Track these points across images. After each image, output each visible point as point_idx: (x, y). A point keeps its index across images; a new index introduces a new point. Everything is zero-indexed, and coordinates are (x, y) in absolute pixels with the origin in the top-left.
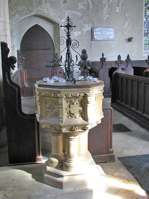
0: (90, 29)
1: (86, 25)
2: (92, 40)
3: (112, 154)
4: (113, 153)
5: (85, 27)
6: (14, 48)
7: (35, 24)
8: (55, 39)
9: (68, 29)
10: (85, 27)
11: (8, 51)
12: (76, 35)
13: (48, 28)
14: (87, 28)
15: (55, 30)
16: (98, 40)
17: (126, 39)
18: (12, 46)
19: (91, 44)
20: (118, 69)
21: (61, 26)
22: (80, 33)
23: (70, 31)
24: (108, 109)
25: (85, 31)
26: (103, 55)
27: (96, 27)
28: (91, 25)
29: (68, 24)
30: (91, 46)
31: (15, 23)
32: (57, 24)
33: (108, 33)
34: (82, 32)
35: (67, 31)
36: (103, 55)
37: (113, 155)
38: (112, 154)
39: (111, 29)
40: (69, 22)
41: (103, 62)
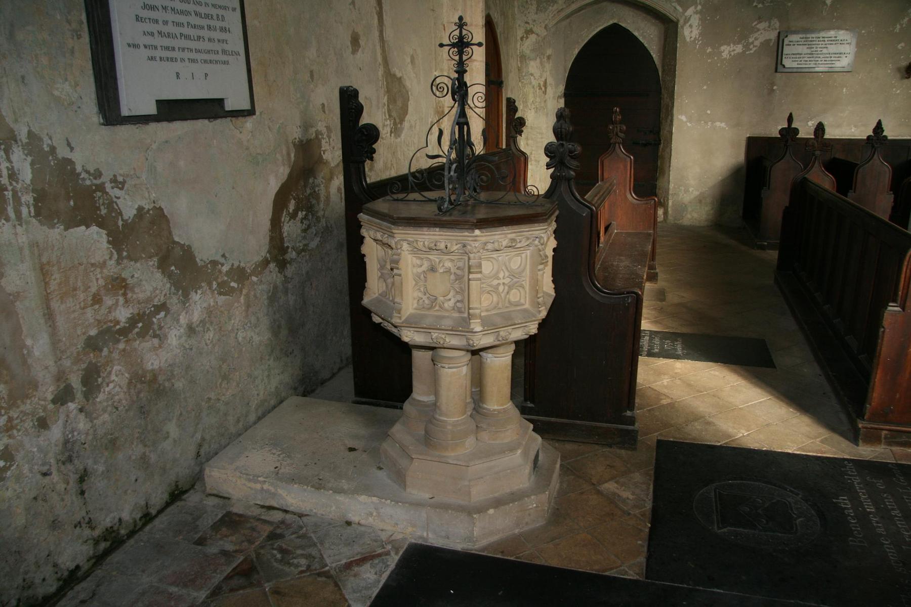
0: (773, 35)
1: (762, 26)
2: (776, 71)
3: (631, 428)
4: (633, 424)
5: (758, 30)
6: (546, 88)
7: (611, 22)
8: (663, 66)
9: (461, 53)
10: (758, 30)
11: (359, 109)
12: (725, 55)
13: (647, 34)
14: (764, 33)
15: (665, 40)
16: (795, 70)
17: (899, 70)
18: (542, 83)
19: (773, 84)
20: (812, 166)
21: (480, 45)
22: (739, 49)
23: (465, 58)
24: (628, 293)
25: (757, 43)
26: (790, 119)
27: (793, 29)
28: (777, 25)
29: (461, 38)
30: (773, 91)
31: (554, 22)
32: (672, 21)
33: (833, 49)
34: (747, 47)
35: (457, 58)
36: (790, 119)
37: (633, 431)
38: (631, 428)
39: (842, 35)
40: (464, 32)
41: (787, 141)
